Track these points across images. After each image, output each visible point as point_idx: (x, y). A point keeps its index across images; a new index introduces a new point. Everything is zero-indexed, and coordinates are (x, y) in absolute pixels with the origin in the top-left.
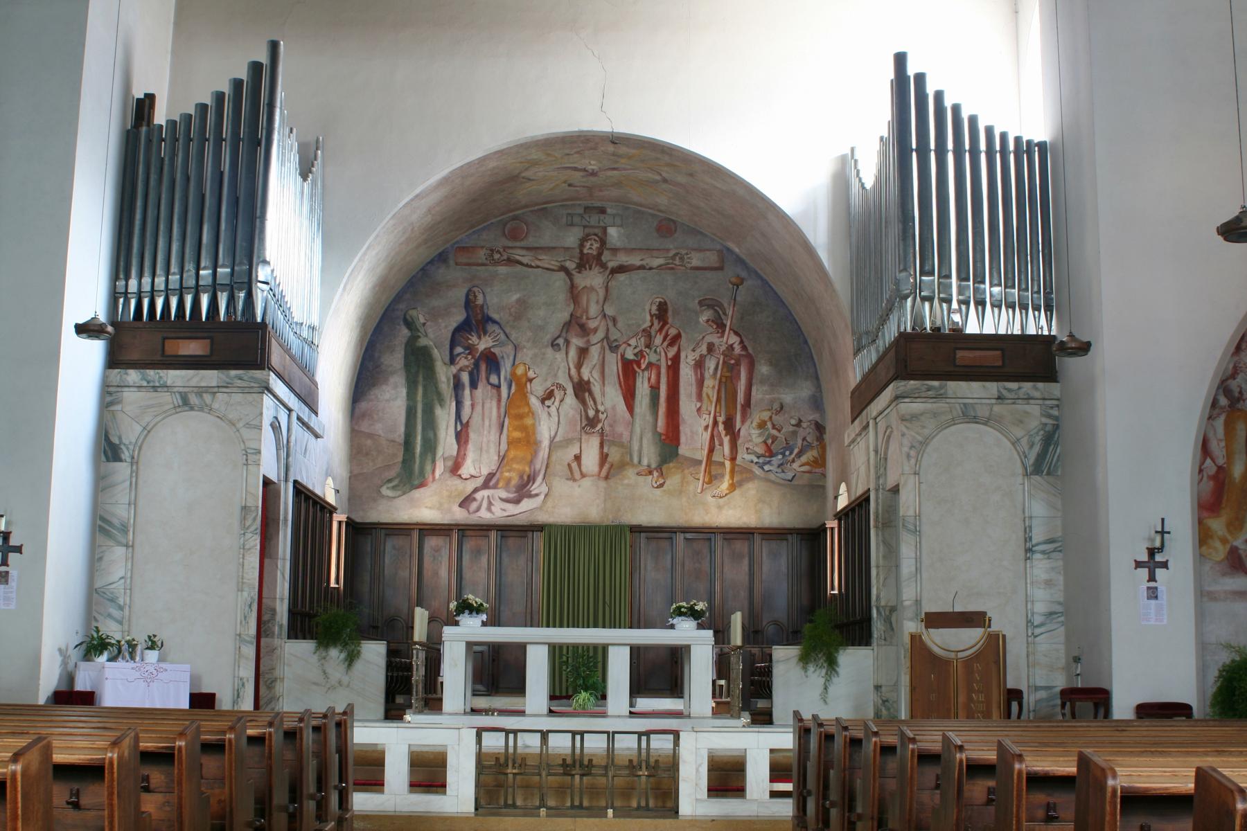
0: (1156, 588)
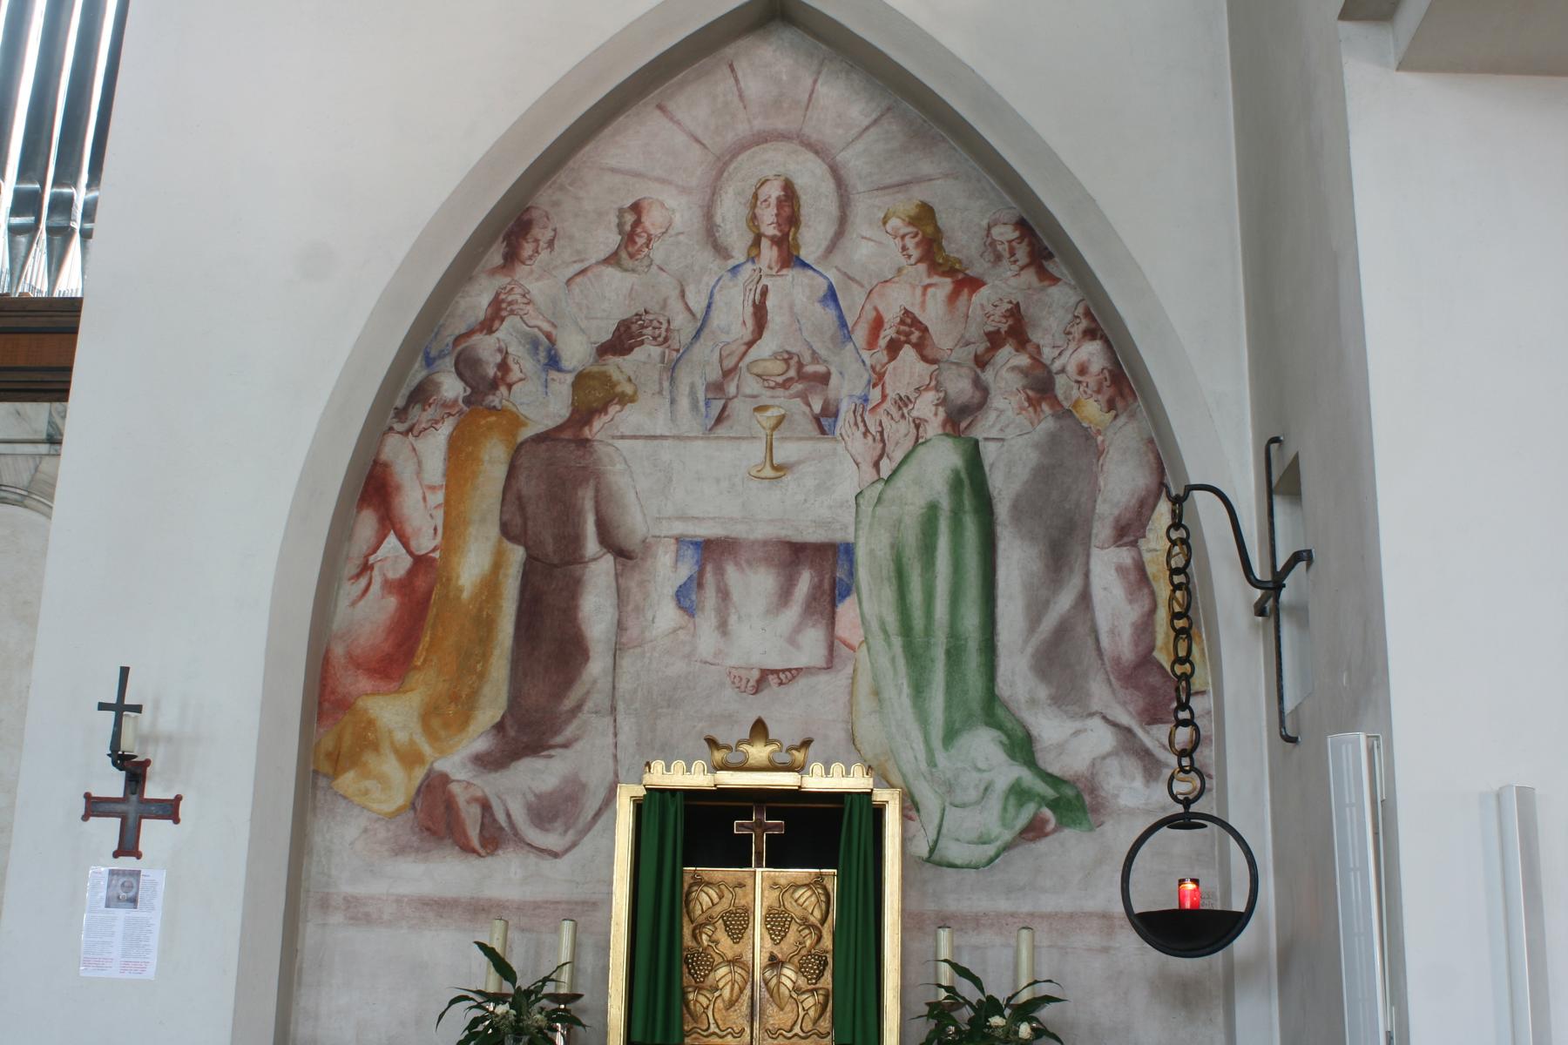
0: (136, 874)
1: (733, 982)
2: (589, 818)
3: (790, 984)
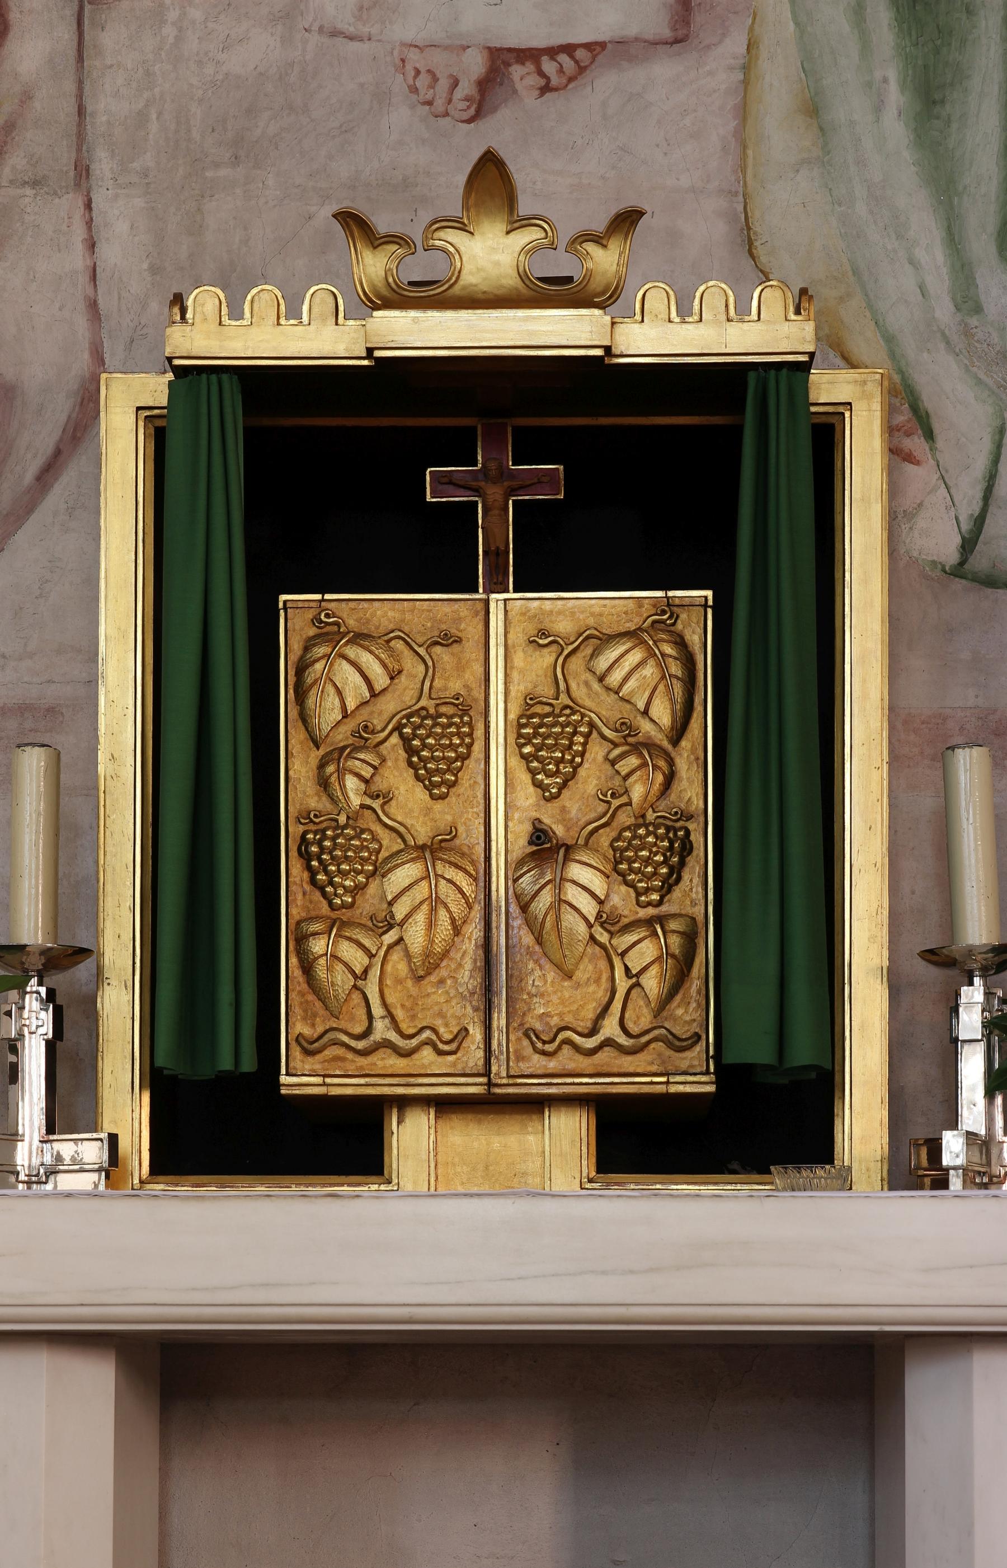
1: (435, 902)
2: (29, 477)
3: (589, 907)
